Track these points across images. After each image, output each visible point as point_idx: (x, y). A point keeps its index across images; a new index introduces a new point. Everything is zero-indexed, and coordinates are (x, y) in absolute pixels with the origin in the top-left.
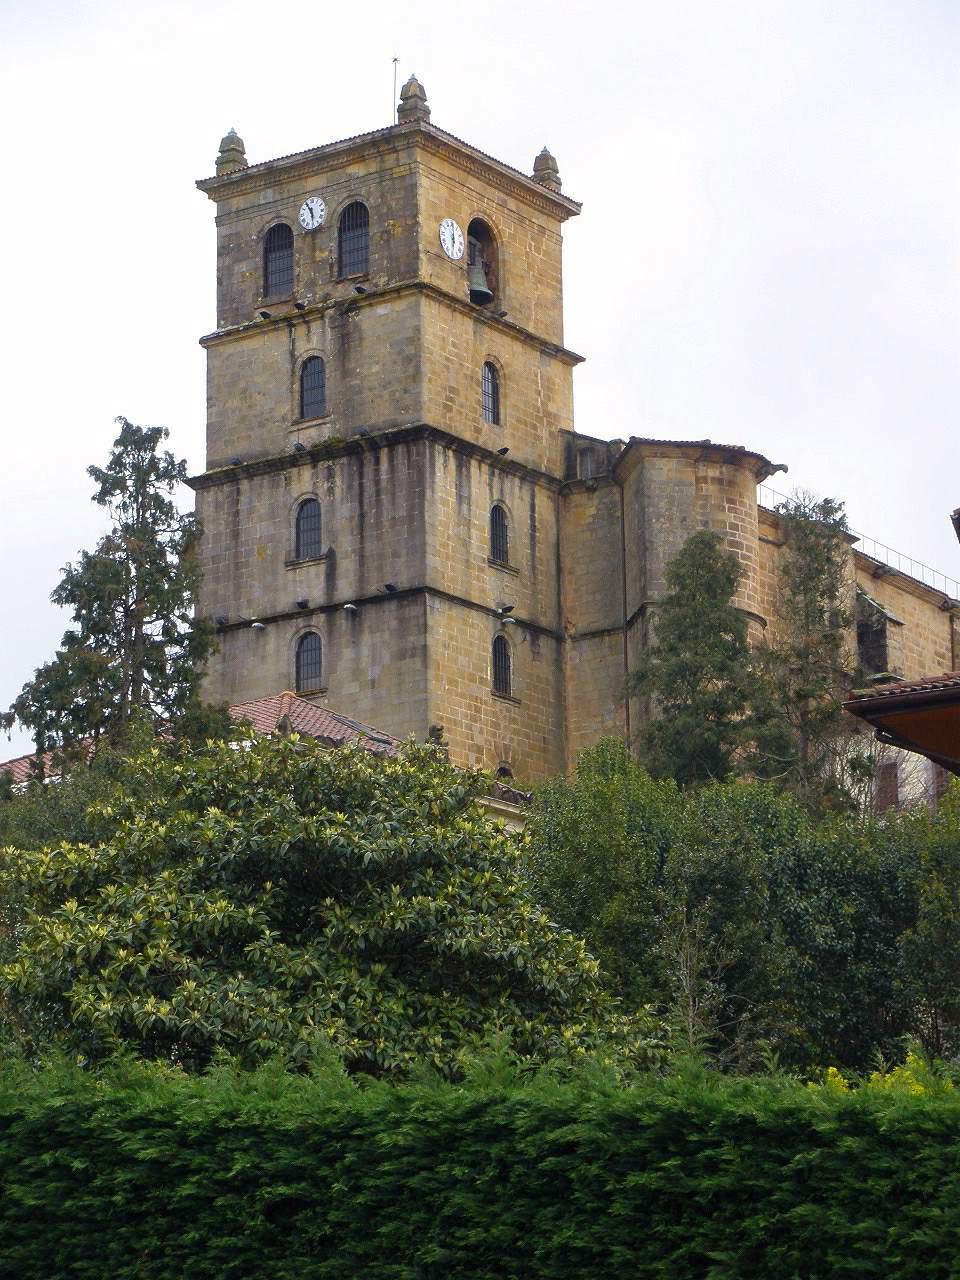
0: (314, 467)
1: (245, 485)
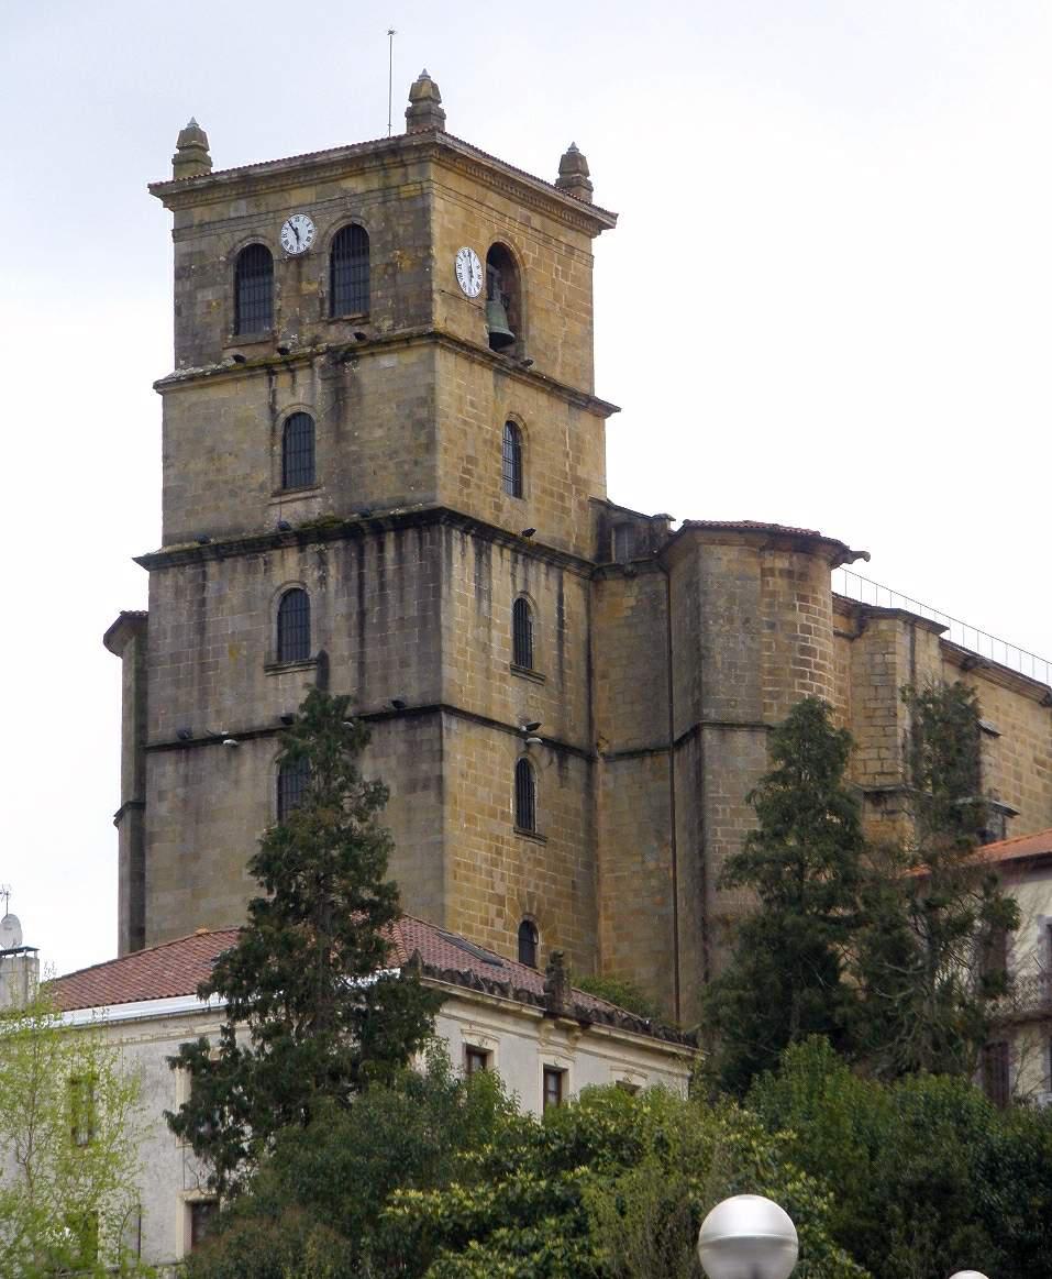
0: (302, 550)
1: (212, 568)
